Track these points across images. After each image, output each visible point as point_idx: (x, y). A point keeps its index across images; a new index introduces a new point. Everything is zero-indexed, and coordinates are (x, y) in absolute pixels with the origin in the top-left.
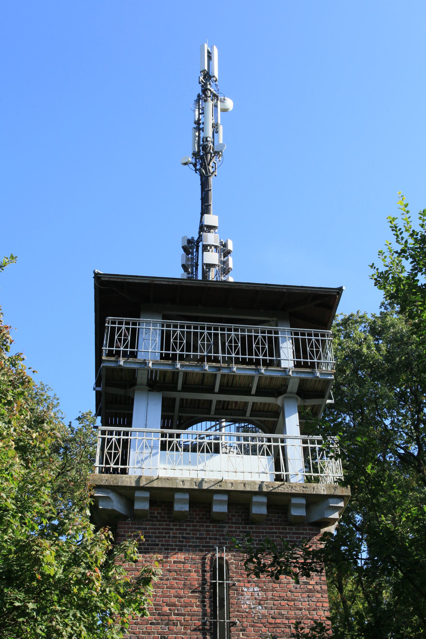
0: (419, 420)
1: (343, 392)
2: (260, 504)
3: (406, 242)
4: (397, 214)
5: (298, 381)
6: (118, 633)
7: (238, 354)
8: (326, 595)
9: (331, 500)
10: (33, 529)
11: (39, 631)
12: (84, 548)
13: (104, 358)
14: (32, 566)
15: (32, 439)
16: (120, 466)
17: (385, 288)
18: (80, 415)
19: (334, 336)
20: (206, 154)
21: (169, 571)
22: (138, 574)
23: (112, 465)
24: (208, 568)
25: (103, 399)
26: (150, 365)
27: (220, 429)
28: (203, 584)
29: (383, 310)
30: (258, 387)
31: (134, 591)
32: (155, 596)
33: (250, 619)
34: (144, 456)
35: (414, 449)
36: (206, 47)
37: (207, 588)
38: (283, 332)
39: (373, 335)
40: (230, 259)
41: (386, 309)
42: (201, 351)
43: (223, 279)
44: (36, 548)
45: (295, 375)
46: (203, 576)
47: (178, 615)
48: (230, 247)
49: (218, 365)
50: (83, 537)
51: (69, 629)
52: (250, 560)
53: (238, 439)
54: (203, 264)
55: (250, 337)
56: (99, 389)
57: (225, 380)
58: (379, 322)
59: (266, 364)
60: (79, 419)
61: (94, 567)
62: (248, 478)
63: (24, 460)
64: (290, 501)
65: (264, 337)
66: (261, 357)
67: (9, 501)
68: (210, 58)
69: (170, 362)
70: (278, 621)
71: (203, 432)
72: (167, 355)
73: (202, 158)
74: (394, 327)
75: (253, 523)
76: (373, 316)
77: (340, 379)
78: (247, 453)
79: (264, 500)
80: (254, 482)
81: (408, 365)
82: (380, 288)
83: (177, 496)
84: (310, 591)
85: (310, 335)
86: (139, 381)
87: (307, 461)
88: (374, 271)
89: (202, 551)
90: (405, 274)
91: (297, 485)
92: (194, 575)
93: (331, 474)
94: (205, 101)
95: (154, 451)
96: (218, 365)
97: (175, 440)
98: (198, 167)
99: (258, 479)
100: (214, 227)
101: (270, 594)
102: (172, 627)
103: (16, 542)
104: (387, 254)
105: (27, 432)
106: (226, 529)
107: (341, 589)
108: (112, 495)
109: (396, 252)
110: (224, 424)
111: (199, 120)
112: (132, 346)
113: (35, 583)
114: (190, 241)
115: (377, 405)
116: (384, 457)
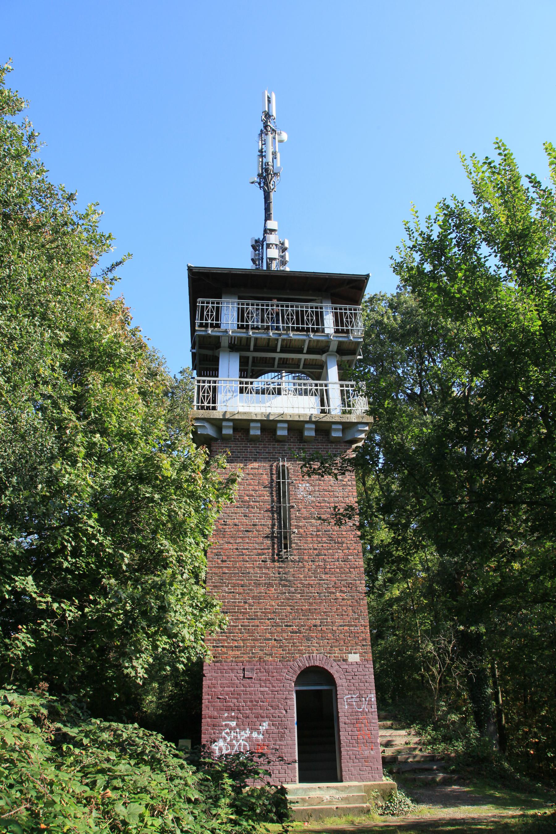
0: (422, 370)
1: (370, 350)
2: (310, 429)
3: (416, 240)
4: (410, 218)
5: (336, 343)
6: (216, 513)
7: (293, 324)
8: (355, 488)
9: (359, 426)
10: (154, 447)
11: (163, 511)
12: (190, 459)
13: (197, 328)
14: (156, 471)
15: (150, 387)
16: (211, 405)
17: (400, 274)
18: (181, 370)
19: (363, 310)
20: (268, 175)
21: (248, 474)
22: (227, 476)
23: (206, 404)
24: (274, 472)
25: (197, 357)
26: (230, 333)
27: (281, 378)
28: (272, 482)
29: (398, 291)
30: (308, 348)
31: (224, 487)
32: (239, 490)
33: (303, 504)
34: (228, 397)
35: (417, 390)
36: (266, 94)
37: (274, 484)
38: (326, 307)
39: (392, 309)
40: (287, 254)
41: (401, 290)
42: (267, 323)
43: (282, 269)
44: (157, 459)
45: (335, 339)
46: (271, 477)
47: (255, 502)
48: (287, 245)
49: (280, 332)
50: (188, 452)
51: (182, 510)
52: (305, 465)
53: (294, 384)
55: (302, 311)
56: (194, 351)
58: (395, 300)
59: (313, 330)
60: (181, 372)
61: (197, 471)
62: (302, 412)
63: (146, 401)
64: (331, 427)
65: (312, 312)
66: (310, 326)
67: (137, 428)
68: (269, 101)
69: (244, 330)
70: (322, 504)
71: (269, 380)
72: (242, 325)
73: (265, 178)
74: (406, 303)
75: (305, 442)
76: (392, 295)
77: (367, 341)
78: (300, 394)
79: (313, 426)
80: (306, 415)
81: (415, 331)
82: (397, 274)
83: (252, 425)
84: (344, 485)
85: (345, 309)
86: (222, 344)
87: (343, 400)
88: (393, 262)
89: (270, 461)
90: (415, 264)
91: (336, 415)
92: (265, 477)
93: (360, 408)
94: (266, 134)
95: (235, 394)
97: (250, 386)
98: (262, 185)
99: (308, 412)
100: (274, 230)
101: (317, 489)
102: (251, 509)
103: (144, 456)
104: (402, 249)
105: (146, 382)
106: (287, 446)
107: (364, 484)
108: (206, 424)
109: (409, 247)
110: (284, 374)
111: (262, 149)
112: (217, 319)
113: (158, 482)
114: (257, 241)
115: (393, 359)
116: (397, 396)
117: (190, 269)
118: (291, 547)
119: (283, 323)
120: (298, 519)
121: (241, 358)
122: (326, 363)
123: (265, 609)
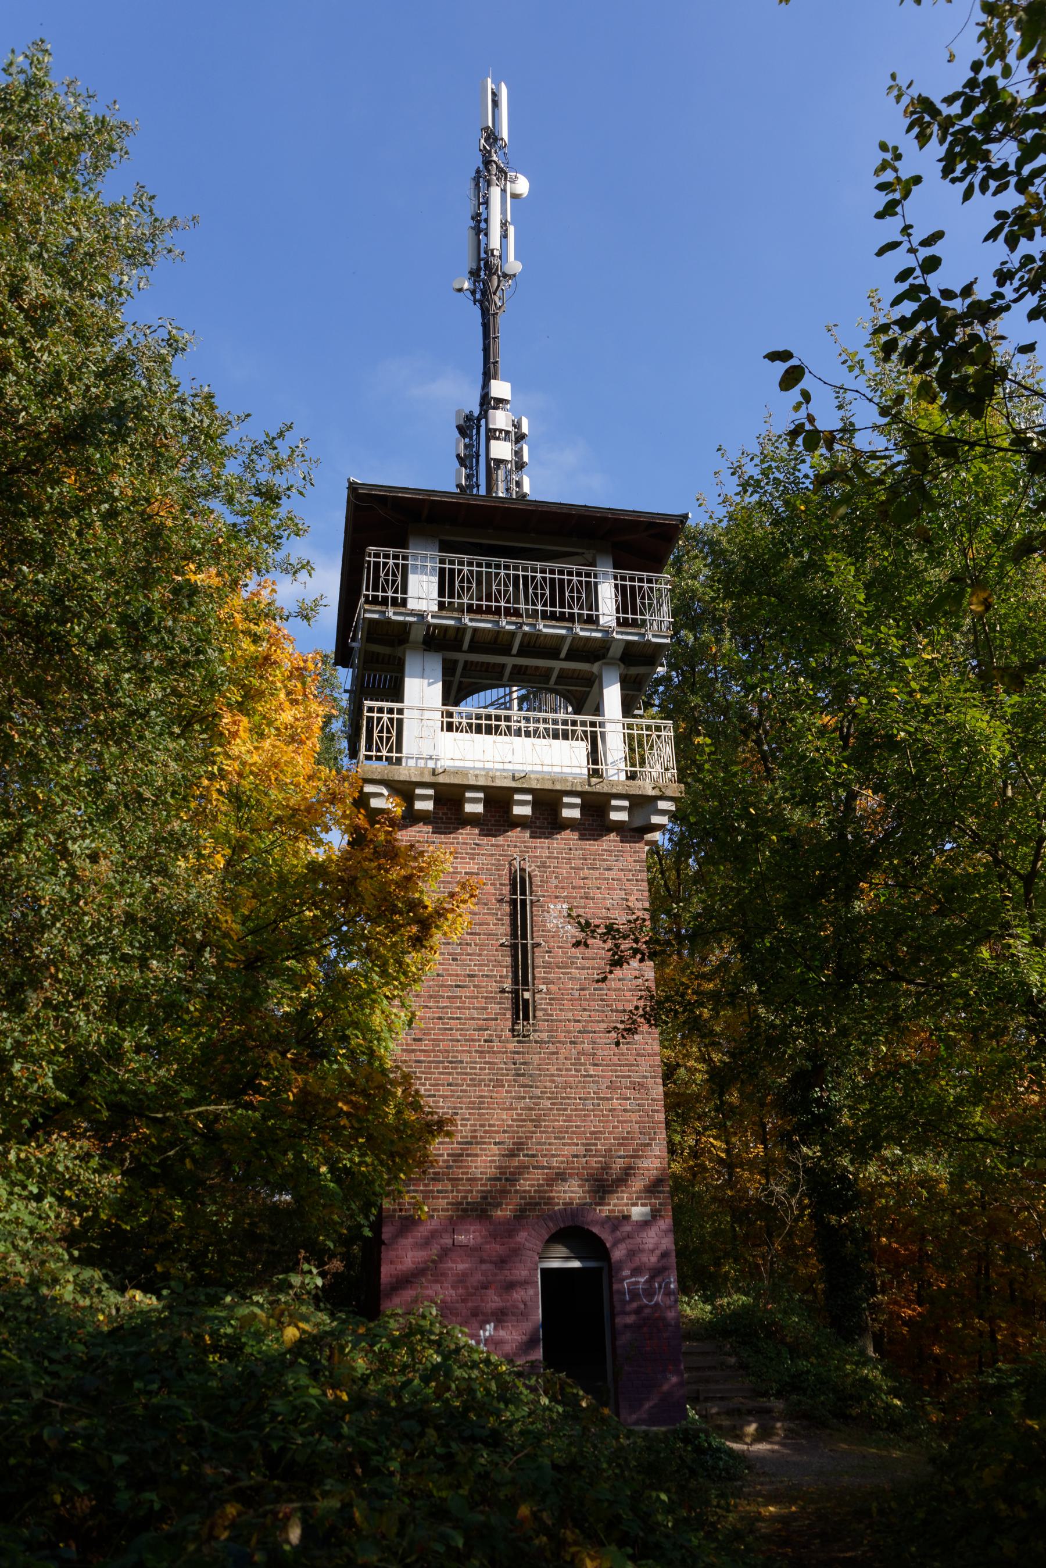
5: (622, 645)
7: (545, 605)
20: (490, 276)
36: (490, 85)
45: (619, 637)
48: (525, 429)
54: (488, 459)
57: (526, 639)
68: (496, 104)
86: (412, 637)
96: (520, 620)
114: (469, 418)
117: (353, 487)
118: (534, 1017)
119: (527, 603)
120: (548, 966)
121: (445, 661)
122: (600, 677)
123: (490, 1125)
